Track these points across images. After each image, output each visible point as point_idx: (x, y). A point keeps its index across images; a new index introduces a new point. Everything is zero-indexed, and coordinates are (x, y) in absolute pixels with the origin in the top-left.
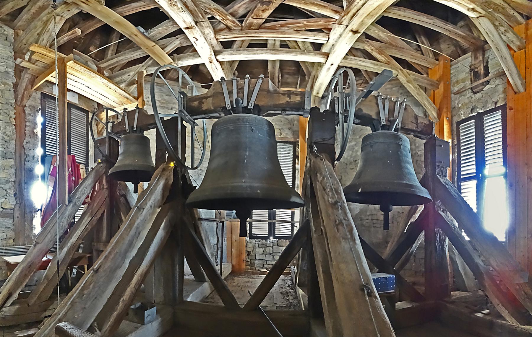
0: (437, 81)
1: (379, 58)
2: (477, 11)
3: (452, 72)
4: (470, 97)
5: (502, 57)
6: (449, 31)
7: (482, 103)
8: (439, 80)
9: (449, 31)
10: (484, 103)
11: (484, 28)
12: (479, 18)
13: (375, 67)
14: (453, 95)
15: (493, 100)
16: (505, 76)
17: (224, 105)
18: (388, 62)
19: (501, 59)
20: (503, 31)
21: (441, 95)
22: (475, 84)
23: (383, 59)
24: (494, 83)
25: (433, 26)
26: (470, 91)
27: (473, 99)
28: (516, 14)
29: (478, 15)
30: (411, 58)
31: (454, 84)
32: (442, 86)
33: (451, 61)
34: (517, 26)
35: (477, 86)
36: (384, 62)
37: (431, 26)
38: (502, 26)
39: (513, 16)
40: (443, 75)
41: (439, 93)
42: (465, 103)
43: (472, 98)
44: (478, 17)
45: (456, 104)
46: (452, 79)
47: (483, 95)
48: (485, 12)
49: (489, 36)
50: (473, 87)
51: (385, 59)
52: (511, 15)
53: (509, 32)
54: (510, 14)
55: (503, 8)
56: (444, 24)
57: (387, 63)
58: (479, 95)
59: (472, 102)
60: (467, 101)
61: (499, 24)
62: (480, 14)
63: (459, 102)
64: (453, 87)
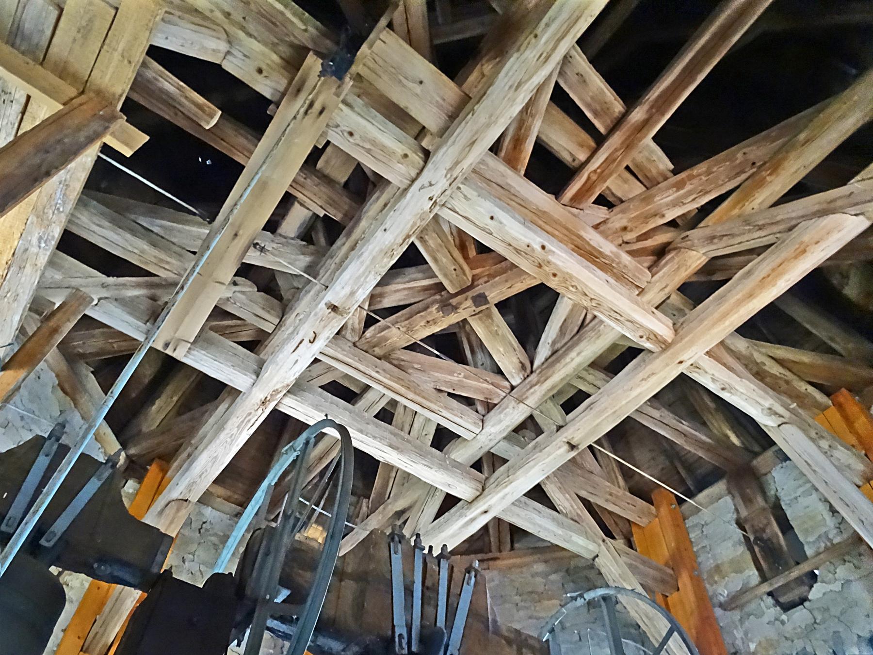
0: (667, 564)
1: (559, 503)
2: (776, 414)
3: (692, 535)
4: (776, 619)
5: (863, 522)
6: (685, 435)
7: (825, 641)
8: (671, 563)
9: (685, 435)
10: (831, 643)
11: (799, 452)
12: (781, 427)
13: (560, 532)
14: (718, 612)
15: (855, 631)
16: (233, 391)
17: (390, 633)
18: (578, 515)
19: (864, 530)
20: (827, 447)
21: (692, 613)
22: (778, 582)
23: (567, 505)
24: (831, 575)
25: (655, 424)
26: (770, 600)
27: (788, 627)
28: (811, 389)
29: (781, 420)
30: (607, 500)
31: (711, 576)
32: (684, 580)
33: (681, 502)
34: (819, 414)
35: (786, 587)
36: (569, 516)
37: (654, 423)
38: (822, 437)
39: (807, 395)
40: (678, 548)
41: (681, 602)
42: (765, 638)
43: (783, 623)
44: (779, 426)
45: (739, 643)
46: (700, 560)
47: (816, 613)
48: (788, 413)
49: (814, 471)
50: (776, 589)
51: (572, 506)
52: (804, 394)
53: (836, 449)
54: (801, 392)
55: (787, 382)
56: (678, 421)
57: (576, 518)
58: (799, 614)
59: (787, 635)
60: (771, 633)
61: (817, 433)
62: (782, 419)
63: (746, 634)
64: (712, 585)
